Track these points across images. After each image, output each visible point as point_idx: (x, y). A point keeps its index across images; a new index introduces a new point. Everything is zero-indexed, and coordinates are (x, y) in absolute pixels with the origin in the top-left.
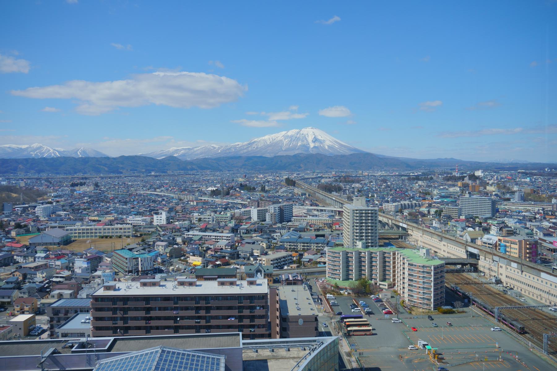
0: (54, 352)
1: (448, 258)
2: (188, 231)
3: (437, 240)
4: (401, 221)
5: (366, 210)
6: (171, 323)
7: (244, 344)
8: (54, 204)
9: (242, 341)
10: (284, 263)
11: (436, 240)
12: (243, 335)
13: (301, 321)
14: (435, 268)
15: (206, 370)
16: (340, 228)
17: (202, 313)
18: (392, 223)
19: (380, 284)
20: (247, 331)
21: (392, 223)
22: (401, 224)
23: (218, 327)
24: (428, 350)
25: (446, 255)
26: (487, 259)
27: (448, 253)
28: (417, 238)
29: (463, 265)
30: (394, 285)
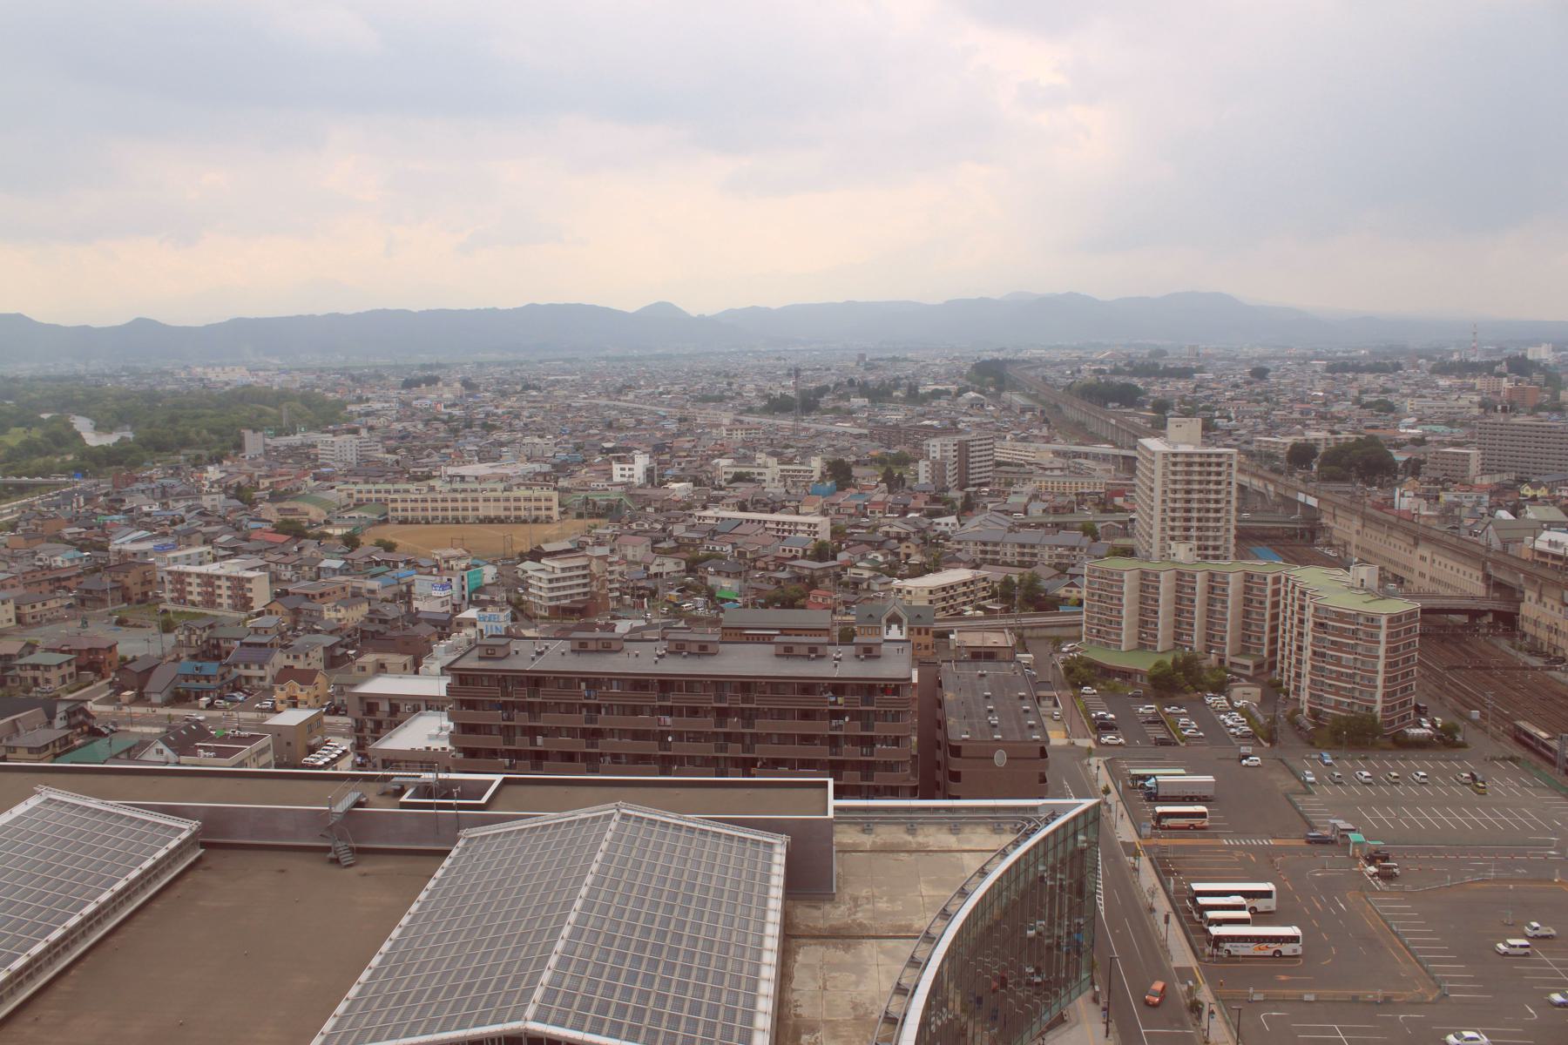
0: (358, 804)
1: (1433, 595)
2: (705, 508)
3: (1404, 545)
4: (1302, 487)
5: (1201, 455)
6: (651, 747)
7: (836, 809)
8: (364, 433)
9: (832, 802)
10: (964, 599)
11: (1398, 543)
12: (836, 787)
13: (1000, 758)
14: (1390, 621)
15: (6, 485)
16: (1127, 506)
17: (734, 725)
18: (1278, 494)
19: (1232, 664)
20: (852, 777)
21: (1278, 494)
22: (1301, 497)
23: (774, 764)
24: (1355, 843)
25: (1426, 585)
26: (1545, 599)
27: (1432, 579)
28: (1346, 538)
29: (1475, 614)
30: (1273, 666)
